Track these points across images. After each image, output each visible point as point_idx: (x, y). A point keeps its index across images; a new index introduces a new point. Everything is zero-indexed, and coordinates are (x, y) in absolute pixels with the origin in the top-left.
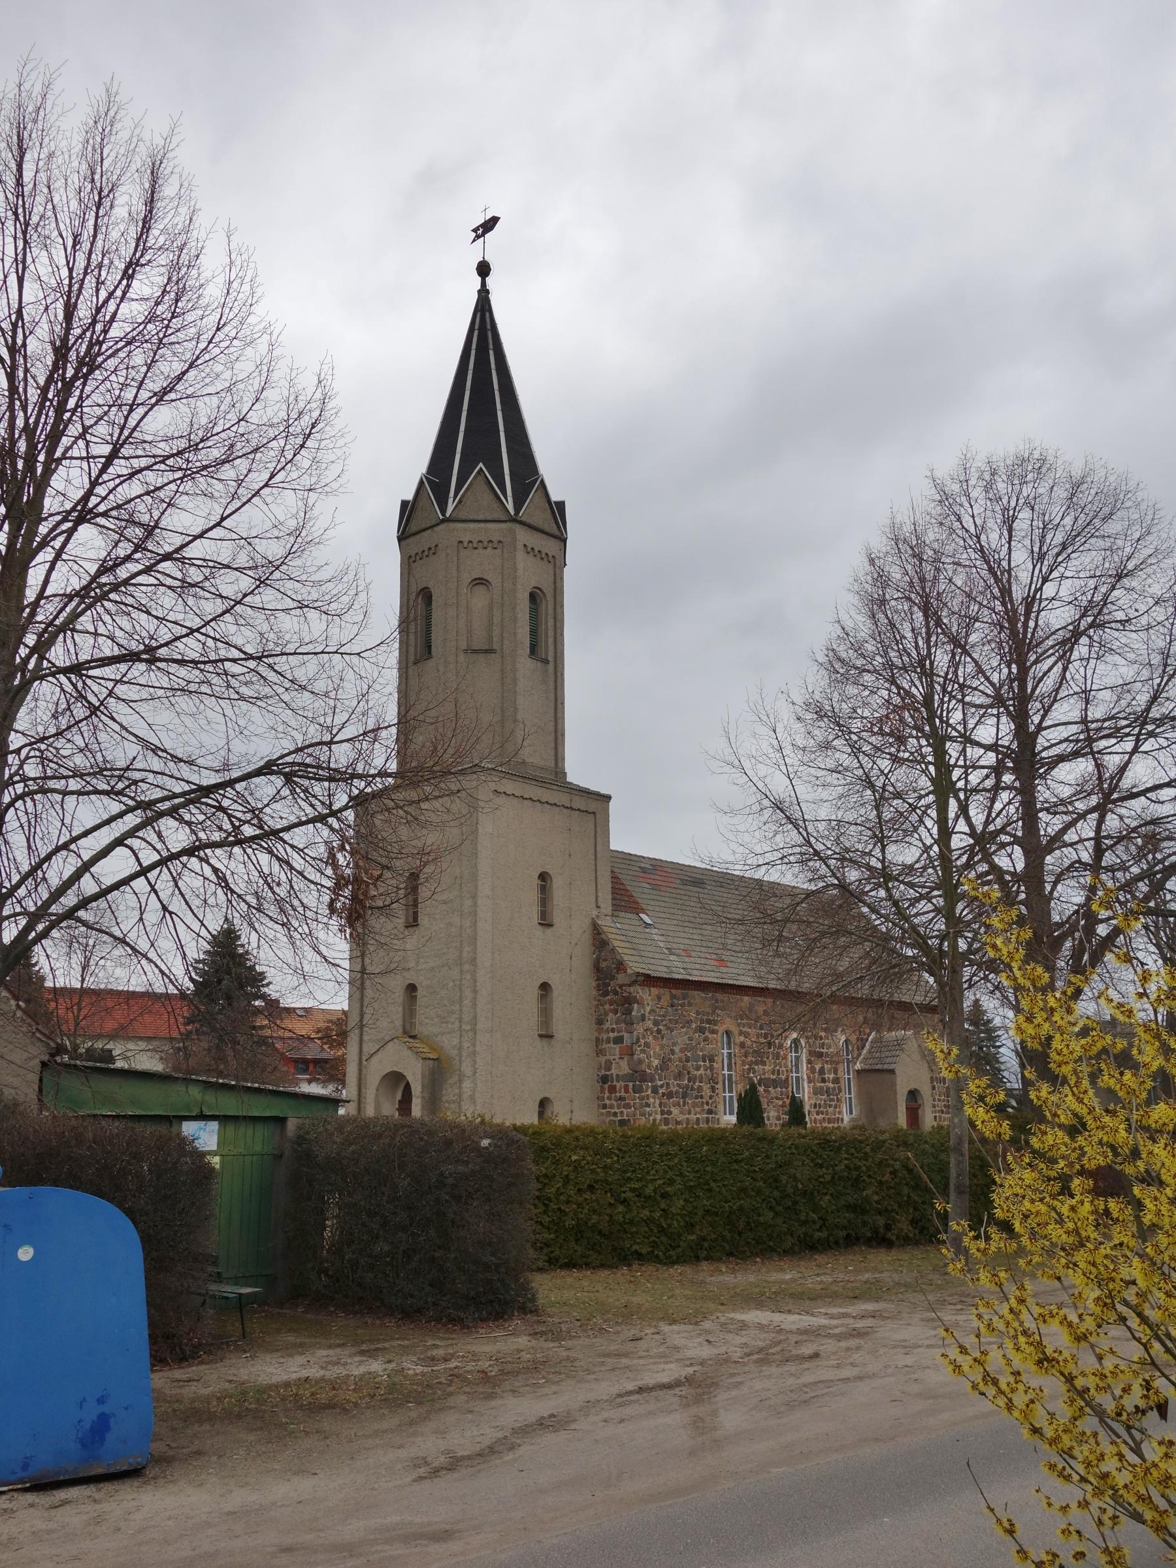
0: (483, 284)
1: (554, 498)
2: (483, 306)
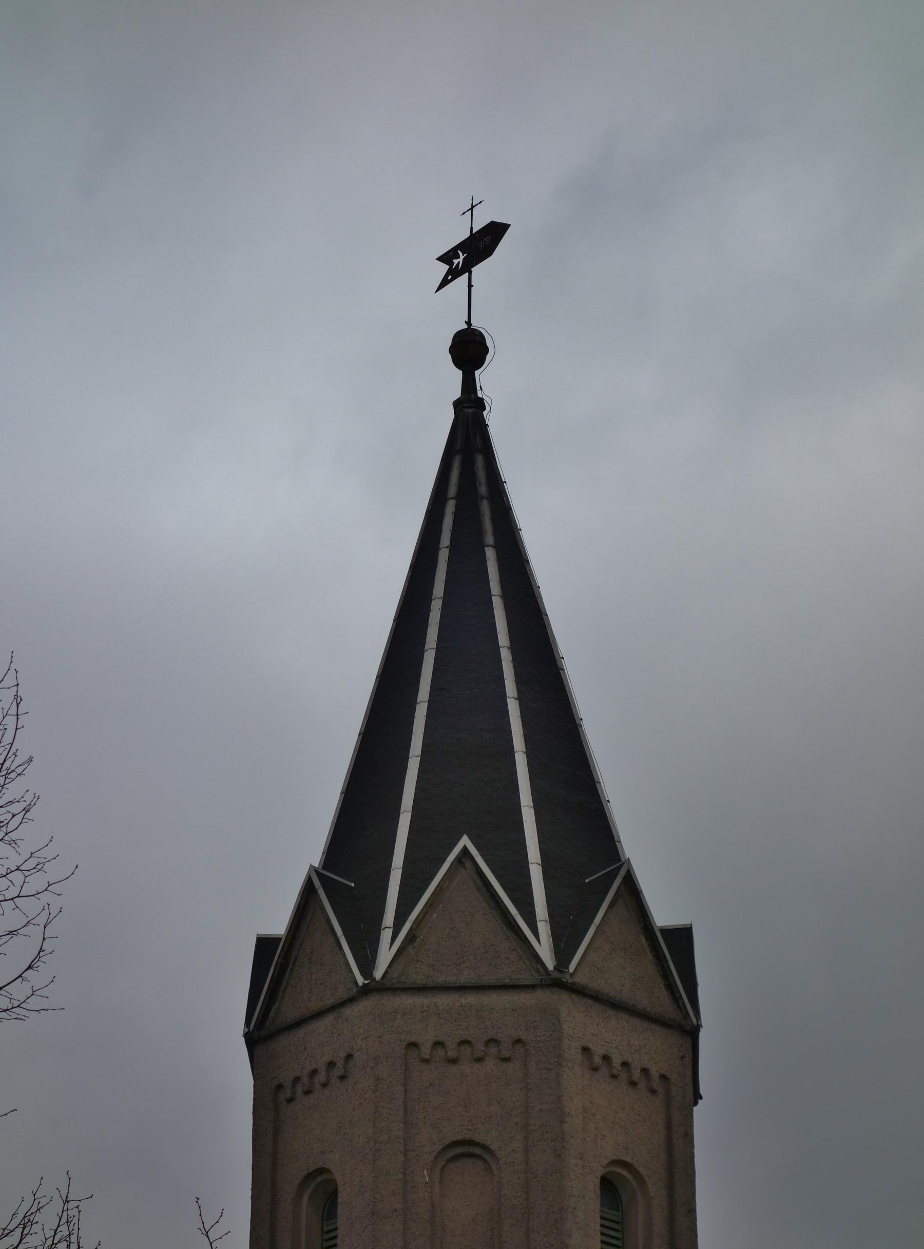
0: (469, 385)
1: (663, 916)
2: (470, 412)
